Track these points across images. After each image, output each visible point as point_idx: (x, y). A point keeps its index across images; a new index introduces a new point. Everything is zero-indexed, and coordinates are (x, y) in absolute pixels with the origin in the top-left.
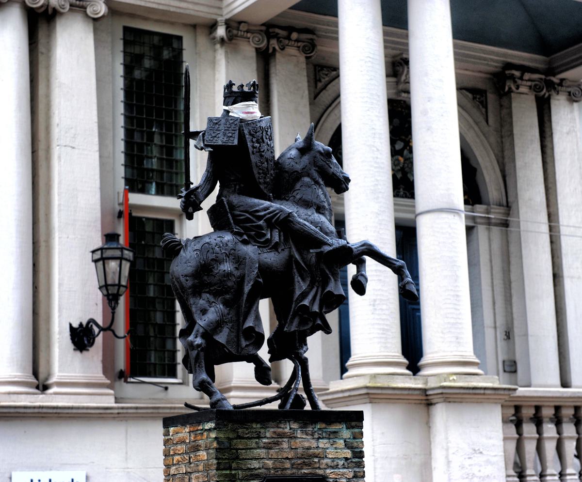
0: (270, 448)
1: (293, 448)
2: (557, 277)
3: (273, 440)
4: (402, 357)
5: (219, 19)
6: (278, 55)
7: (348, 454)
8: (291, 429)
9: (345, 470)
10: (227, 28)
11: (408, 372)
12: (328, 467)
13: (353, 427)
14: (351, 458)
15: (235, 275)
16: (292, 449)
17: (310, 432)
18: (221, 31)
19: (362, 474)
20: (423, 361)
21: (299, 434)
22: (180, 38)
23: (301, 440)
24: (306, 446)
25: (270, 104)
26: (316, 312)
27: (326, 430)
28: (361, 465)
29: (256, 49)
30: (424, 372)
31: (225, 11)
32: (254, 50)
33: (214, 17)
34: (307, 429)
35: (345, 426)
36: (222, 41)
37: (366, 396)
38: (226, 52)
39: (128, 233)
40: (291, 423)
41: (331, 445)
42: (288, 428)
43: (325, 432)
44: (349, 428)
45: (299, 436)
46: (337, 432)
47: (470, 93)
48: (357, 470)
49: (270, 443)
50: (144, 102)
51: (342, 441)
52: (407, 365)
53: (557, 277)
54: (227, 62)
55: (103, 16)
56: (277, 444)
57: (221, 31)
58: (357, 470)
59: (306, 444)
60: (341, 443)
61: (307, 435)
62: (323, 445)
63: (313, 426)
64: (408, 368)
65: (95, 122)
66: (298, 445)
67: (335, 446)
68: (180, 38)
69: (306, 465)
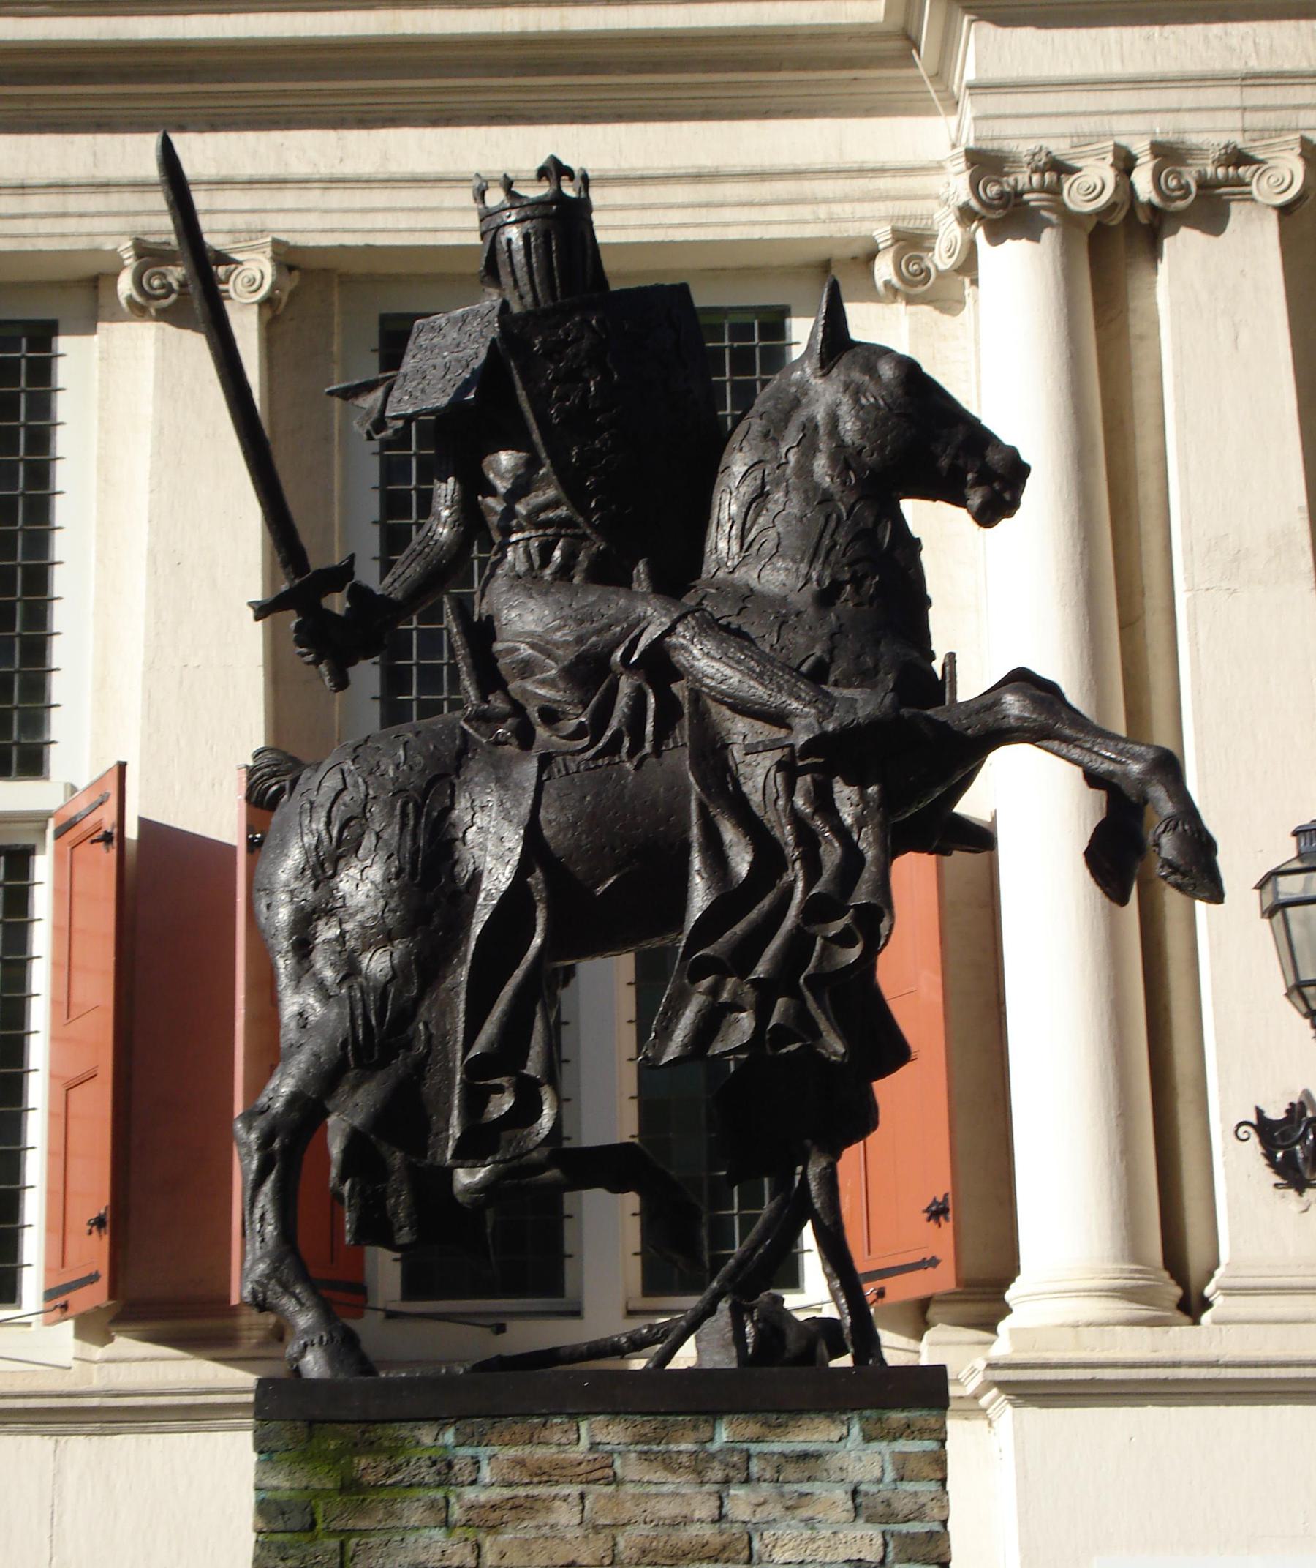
0: (493, 1529)
1: (605, 1526)
2: (642, 180)
3: (507, 1493)
8: (594, 1446)
13: (894, 1436)
15: (674, 640)
16: (596, 1529)
17: (684, 1459)
23: (638, 1490)
24: (663, 1514)
25: (379, 44)
26: (848, 783)
27: (764, 1447)
34: (673, 1447)
35: (856, 1430)
39: (268, 535)
41: (788, 1508)
42: (585, 1443)
43: (762, 1455)
46: (817, 1456)
47: (795, 783)
49: (494, 1507)
50: (726, 337)
51: (841, 1495)
52: (1115, 906)
53: (642, 180)
56: (520, 1507)
59: (668, 1509)
61: (674, 1471)
62: (749, 1511)
63: (704, 1432)
65: (1300, 508)
66: (630, 1510)
67: (805, 1513)
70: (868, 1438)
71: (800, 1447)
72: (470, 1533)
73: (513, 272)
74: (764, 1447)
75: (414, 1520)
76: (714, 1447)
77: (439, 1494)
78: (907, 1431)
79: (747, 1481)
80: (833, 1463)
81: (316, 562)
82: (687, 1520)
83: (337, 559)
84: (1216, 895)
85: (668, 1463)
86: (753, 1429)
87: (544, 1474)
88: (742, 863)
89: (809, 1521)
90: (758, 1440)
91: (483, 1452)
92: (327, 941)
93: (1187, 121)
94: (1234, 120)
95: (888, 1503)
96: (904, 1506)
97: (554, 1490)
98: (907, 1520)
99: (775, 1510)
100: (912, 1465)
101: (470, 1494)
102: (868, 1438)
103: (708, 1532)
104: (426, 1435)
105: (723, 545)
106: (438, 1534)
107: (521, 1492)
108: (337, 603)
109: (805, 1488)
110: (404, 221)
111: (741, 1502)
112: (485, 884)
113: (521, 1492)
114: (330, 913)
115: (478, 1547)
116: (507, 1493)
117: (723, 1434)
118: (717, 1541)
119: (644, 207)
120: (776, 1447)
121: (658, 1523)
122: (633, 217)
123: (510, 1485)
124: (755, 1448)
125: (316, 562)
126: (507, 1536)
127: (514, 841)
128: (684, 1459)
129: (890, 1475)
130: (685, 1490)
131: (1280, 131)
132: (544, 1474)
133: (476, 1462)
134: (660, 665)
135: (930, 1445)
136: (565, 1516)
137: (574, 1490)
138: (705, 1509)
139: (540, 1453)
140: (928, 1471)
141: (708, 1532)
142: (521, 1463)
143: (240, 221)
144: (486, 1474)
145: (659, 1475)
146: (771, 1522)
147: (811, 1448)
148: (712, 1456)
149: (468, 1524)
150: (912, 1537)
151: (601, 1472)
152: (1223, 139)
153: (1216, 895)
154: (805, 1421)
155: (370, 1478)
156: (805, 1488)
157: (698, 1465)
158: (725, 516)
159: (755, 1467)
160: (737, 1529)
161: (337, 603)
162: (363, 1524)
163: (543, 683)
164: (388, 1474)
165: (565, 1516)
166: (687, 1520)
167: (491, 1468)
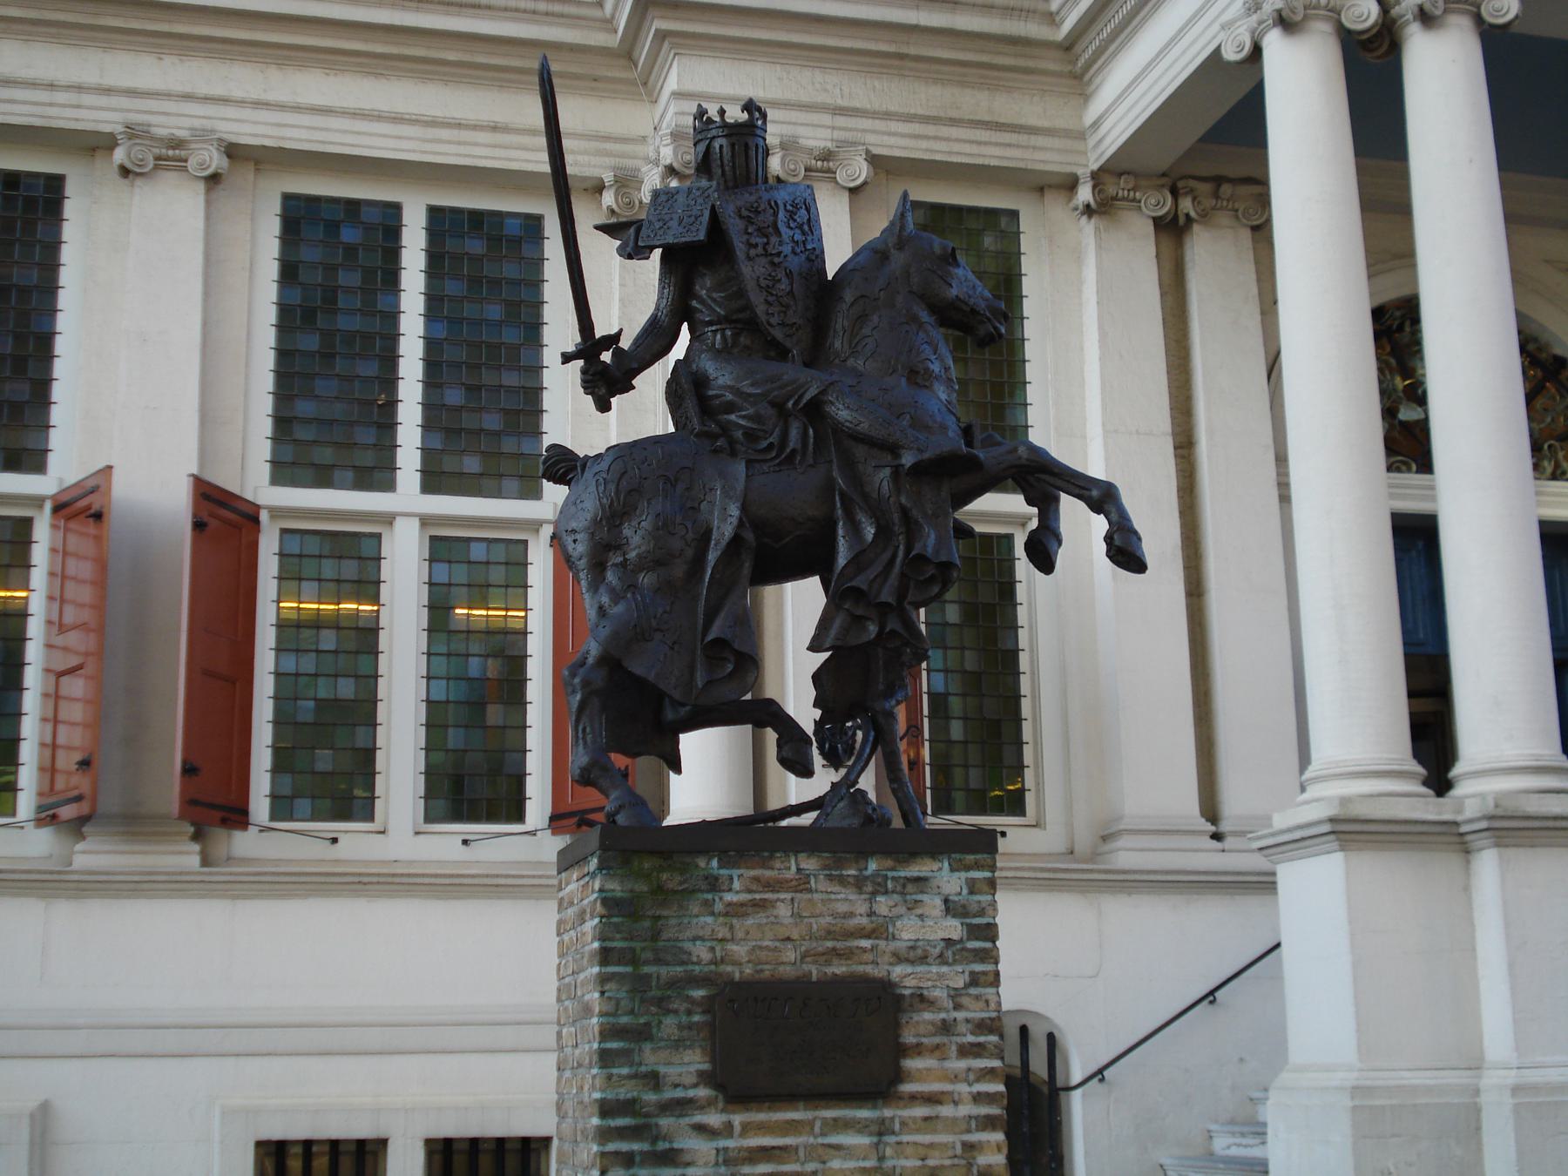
2: (459, 126)
3: (749, 896)
4: (1414, 762)
5: (1080, 172)
6: (1196, 227)
7: (953, 928)
8: (799, 870)
9: (945, 969)
10: (1094, 187)
11: (1424, 790)
12: (899, 958)
13: (968, 868)
14: (961, 941)
17: (851, 880)
18: (1085, 194)
19: (991, 978)
20: (1457, 771)
21: (820, 884)
22: (1014, 215)
23: (825, 896)
27: (895, 874)
28: (991, 956)
29: (1155, 219)
30: (1457, 791)
31: (1092, 157)
32: (1151, 222)
33: (1068, 169)
35: (946, 864)
36: (1088, 210)
37: (1332, 837)
38: (1097, 229)
40: (802, 856)
42: (794, 868)
43: (893, 878)
44: (958, 870)
45: (821, 888)
48: (978, 967)
51: (938, 902)
53: (459, 126)
54: (1099, 247)
55: (865, 183)
56: (761, 905)
57: (1085, 194)
58: (978, 967)
59: (842, 908)
60: (933, 904)
63: (862, 865)
64: (1426, 783)
67: (919, 911)
68: (1014, 215)
69: (839, 955)
70: (952, 870)
71: (916, 874)
72: (727, 920)
73: (722, 165)
74: (895, 874)
75: (696, 910)
76: (869, 872)
77: (709, 896)
78: (977, 866)
79: (886, 892)
80: (934, 883)
81: (600, 332)
82: (851, 915)
83: (614, 331)
84: (678, 770)
85: (842, 881)
86: (889, 863)
87: (770, 886)
88: (870, 532)
89: (921, 917)
90: (893, 869)
91: (735, 873)
92: (615, 565)
93: (801, 131)
94: (827, 133)
95: (964, 906)
96: (974, 908)
97: (775, 896)
98: (975, 916)
99: (902, 910)
100: (978, 886)
101: (728, 897)
102: (952, 870)
103: (864, 921)
104: (702, 863)
105: (838, 344)
106: (709, 920)
107: (757, 896)
108: (606, 357)
109: (919, 897)
110: (304, 134)
111: (883, 904)
112: (715, 535)
113: (757, 896)
114: (618, 547)
115: (732, 927)
116: (749, 896)
117: (873, 866)
118: (870, 927)
119: (459, 143)
120: (902, 874)
121: (834, 915)
122: (453, 149)
123: (750, 891)
124: (890, 874)
125: (600, 332)
126: (750, 921)
127: (734, 511)
128: (851, 880)
129: (965, 891)
130: (852, 897)
131: (854, 144)
132: (770, 886)
133: (731, 878)
134: (815, 411)
135: (988, 874)
136: (783, 911)
137: (788, 896)
138: (862, 908)
139: (768, 873)
140: (986, 888)
141: (864, 921)
142: (756, 879)
143: (197, 123)
144: (736, 885)
145: (837, 889)
146: (900, 917)
147: (922, 875)
148: (867, 878)
149: (726, 914)
150: (978, 926)
151: (802, 884)
152: (822, 144)
153: (678, 770)
154: (919, 860)
155: (670, 885)
156: (919, 897)
157: (859, 884)
158: (839, 327)
159: (890, 885)
160: (881, 920)
161: (606, 357)
162: (665, 913)
163: (743, 417)
164: (681, 883)
165: (783, 911)
166: (851, 915)
167: (738, 884)
